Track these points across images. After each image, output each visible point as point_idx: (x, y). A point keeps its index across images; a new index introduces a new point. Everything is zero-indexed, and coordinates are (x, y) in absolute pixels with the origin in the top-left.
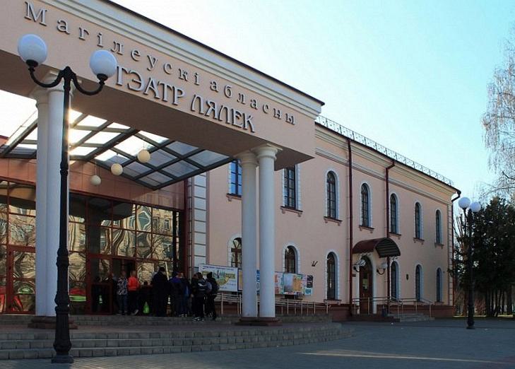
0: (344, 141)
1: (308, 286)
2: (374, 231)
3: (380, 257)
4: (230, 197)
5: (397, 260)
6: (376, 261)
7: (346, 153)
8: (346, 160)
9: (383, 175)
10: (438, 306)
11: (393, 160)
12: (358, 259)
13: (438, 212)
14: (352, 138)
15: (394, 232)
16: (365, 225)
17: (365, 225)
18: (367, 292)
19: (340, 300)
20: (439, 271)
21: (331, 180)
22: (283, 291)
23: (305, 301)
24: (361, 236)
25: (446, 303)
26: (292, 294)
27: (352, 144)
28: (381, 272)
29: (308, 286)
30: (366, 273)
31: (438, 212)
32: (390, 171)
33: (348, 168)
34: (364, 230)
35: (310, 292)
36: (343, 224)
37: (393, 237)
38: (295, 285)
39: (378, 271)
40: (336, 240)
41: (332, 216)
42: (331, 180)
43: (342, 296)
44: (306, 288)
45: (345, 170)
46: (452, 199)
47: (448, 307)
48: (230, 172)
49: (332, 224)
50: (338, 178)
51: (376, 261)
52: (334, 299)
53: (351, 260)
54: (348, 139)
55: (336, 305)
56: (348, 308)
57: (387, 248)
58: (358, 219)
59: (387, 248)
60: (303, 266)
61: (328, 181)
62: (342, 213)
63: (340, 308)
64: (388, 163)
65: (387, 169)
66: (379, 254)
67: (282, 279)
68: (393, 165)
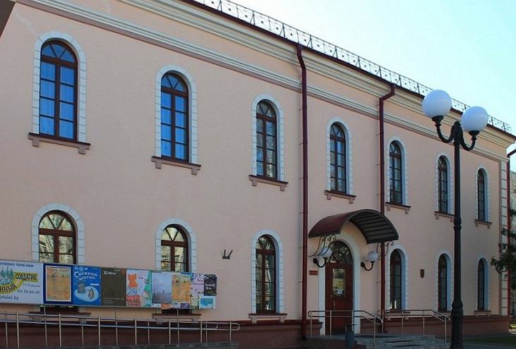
0: (291, 49)
1: (206, 293)
2: (356, 201)
3: (368, 243)
4: (330, 194)
5: (396, 245)
6: (360, 249)
7: (297, 70)
8: (297, 82)
9: (374, 110)
10: (481, 317)
11: (392, 85)
12: (322, 247)
13: (481, 172)
14: (399, 84)
15: (397, 200)
16: (339, 189)
17: (339, 189)
18: (340, 303)
19: (490, 311)
20: (482, 262)
21: (442, 166)
22: (149, 302)
23: (204, 318)
24: (323, 208)
25: (495, 312)
26: (171, 306)
27: (304, 54)
28: (368, 266)
29: (206, 293)
30: (341, 264)
31: (481, 172)
32: (387, 105)
33: (301, 95)
34: (480, 226)
35: (212, 303)
36: (288, 188)
37: (392, 215)
38: (178, 291)
39: (363, 265)
40: (276, 214)
41: (268, 173)
42: (442, 166)
43: (288, 306)
44: (202, 296)
45: (295, 98)
46: (508, 153)
47: (498, 318)
48: (329, 165)
49: (483, 227)
50: (405, 149)
51: (360, 249)
52: (274, 312)
53: (305, 247)
54: (297, 45)
55: (277, 323)
56: (299, 327)
57: (373, 226)
58: (321, 177)
59: (373, 226)
60: (202, 262)
61: (332, 138)
62: (288, 167)
63: (284, 327)
64: (385, 90)
65: (382, 100)
66: (366, 237)
67: (147, 282)
68: (392, 94)
